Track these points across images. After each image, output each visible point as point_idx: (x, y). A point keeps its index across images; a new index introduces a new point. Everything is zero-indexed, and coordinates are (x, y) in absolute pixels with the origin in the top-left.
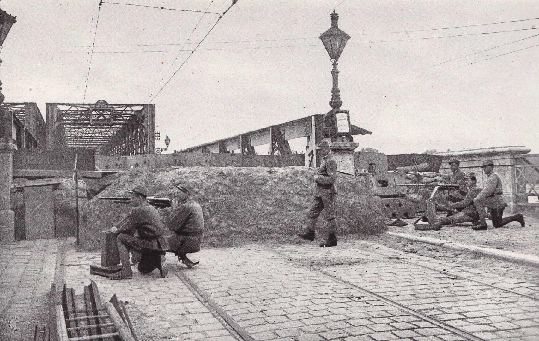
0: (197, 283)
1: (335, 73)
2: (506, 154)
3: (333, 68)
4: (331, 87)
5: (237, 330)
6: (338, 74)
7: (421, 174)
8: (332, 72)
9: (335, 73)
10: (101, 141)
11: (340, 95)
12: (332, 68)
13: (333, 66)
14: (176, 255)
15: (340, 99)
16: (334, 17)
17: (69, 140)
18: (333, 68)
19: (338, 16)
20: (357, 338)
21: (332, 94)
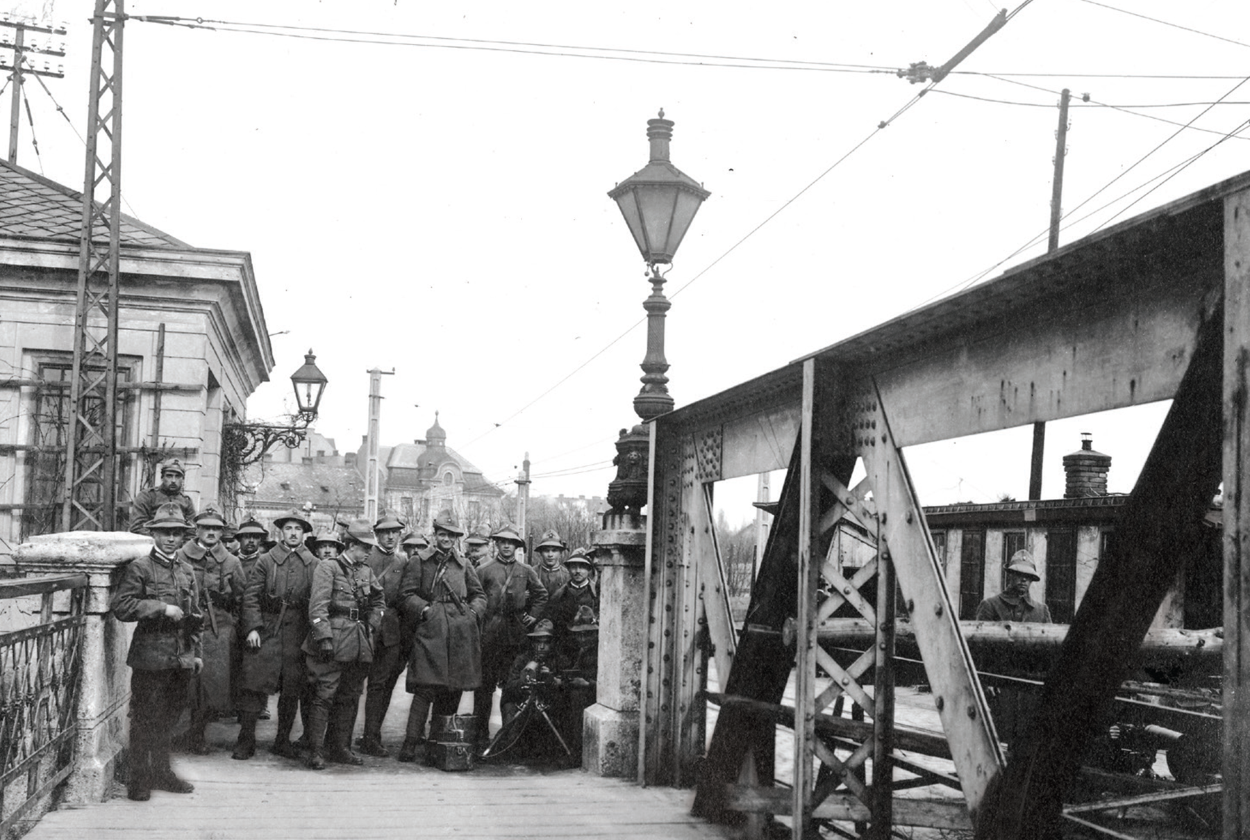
0: (1240, 198)
1: (657, 309)
2: (90, 563)
3: (651, 292)
4: (640, 352)
5: (885, 494)
6: (667, 313)
7: (646, 510)
8: (647, 305)
9: (657, 309)
10: (85, 568)
11: (666, 381)
12: (647, 290)
13: (652, 285)
14: (1014, 500)
15: (666, 391)
16: (660, 130)
17: (37, 564)
18: (651, 292)
19: (671, 135)
20: (807, 778)
21: (643, 374)
